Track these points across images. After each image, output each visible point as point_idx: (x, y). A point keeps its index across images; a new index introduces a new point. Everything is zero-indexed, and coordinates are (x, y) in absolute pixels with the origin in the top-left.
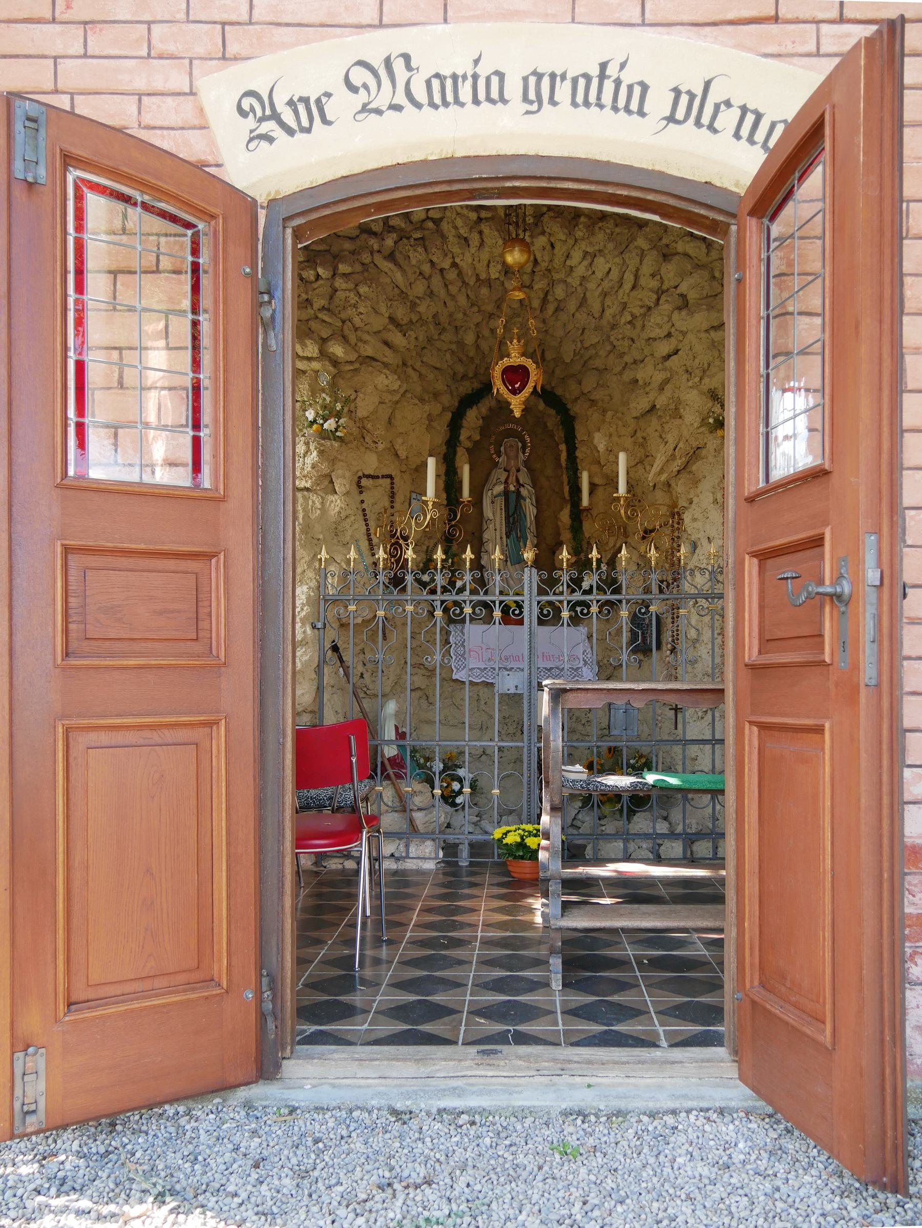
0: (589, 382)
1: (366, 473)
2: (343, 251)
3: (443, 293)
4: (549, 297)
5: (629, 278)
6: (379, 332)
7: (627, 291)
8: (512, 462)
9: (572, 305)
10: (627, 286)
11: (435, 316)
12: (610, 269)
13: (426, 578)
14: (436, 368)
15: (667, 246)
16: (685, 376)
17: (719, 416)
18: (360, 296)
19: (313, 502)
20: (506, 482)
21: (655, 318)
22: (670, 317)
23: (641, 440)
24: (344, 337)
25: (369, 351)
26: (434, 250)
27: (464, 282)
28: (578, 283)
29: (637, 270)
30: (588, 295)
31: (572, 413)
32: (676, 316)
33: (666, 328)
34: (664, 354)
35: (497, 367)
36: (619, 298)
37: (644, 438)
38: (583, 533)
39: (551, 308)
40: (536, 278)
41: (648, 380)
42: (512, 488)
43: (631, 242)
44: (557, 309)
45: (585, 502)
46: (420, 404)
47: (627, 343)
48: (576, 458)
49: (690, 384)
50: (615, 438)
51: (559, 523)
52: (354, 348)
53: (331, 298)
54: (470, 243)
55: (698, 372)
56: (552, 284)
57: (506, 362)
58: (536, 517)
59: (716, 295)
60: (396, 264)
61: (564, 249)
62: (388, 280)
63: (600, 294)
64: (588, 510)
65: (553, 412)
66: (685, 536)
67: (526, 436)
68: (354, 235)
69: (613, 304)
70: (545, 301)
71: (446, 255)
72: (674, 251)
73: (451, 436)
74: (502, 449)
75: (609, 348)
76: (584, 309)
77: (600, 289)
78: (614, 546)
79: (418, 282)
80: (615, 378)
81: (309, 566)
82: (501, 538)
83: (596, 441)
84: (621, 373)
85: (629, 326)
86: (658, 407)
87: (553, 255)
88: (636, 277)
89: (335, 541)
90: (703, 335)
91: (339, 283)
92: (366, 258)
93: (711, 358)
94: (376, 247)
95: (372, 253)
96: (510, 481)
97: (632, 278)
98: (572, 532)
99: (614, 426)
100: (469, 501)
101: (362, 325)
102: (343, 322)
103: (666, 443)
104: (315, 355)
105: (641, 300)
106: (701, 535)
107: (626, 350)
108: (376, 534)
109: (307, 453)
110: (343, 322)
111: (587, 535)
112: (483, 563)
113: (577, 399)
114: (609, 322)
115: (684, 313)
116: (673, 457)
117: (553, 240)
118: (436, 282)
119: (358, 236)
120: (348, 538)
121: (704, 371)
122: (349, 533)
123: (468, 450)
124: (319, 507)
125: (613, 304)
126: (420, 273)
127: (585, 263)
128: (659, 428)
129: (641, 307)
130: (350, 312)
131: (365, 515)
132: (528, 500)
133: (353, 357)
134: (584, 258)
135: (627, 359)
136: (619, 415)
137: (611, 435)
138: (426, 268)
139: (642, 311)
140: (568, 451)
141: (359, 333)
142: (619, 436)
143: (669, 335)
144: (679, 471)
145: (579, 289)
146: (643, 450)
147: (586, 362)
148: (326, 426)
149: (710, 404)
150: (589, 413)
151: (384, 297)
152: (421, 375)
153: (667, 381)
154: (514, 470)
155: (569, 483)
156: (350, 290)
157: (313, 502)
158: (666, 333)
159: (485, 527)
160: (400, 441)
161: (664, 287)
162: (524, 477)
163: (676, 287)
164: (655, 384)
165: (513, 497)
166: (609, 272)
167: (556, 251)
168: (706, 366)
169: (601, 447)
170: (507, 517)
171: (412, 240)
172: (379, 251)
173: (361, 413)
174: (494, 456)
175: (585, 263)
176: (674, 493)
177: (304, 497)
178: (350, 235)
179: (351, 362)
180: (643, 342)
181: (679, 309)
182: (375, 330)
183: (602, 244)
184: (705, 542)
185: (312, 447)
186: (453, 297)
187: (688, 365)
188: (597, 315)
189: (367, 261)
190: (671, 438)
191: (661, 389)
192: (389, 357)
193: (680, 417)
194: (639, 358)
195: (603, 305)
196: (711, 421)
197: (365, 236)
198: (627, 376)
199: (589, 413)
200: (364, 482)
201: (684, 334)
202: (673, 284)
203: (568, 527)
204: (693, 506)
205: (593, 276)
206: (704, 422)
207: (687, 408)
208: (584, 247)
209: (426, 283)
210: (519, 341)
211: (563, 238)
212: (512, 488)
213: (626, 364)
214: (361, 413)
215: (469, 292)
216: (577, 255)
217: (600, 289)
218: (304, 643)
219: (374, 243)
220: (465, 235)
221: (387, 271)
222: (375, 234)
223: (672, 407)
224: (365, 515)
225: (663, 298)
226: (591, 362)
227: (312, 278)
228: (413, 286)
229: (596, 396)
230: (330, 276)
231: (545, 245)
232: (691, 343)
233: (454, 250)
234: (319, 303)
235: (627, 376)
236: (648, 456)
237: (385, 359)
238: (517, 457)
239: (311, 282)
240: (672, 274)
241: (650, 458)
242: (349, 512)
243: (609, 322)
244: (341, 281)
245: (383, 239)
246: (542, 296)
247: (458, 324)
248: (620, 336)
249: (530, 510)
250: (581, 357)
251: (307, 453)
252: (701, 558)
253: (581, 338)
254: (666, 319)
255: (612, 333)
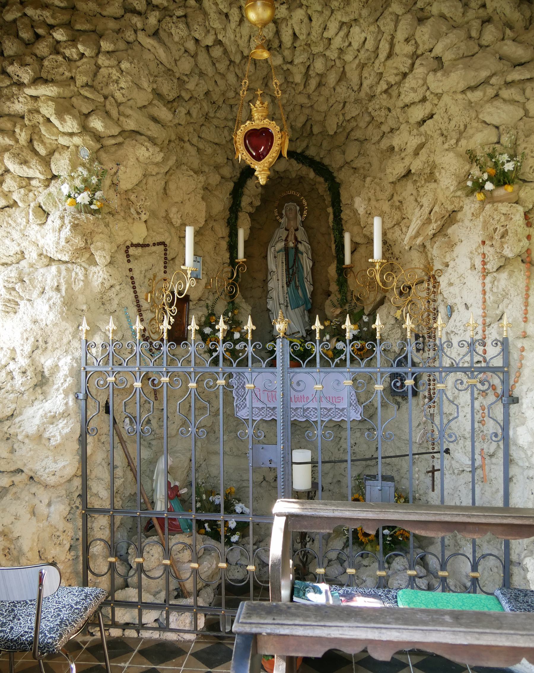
0: (352, 151)
1: (135, 242)
2: (107, 29)
3: (210, 71)
4: (311, 72)
5: (384, 47)
6: (144, 107)
7: (383, 60)
8: (292, 223)
9: (332, 78)
10: (383, 55)
11: (207, 93)
12: (366, 39)
13: (207, 330)
14: (216, 144)
15: (422, 9)
16: (441, 139)
17: (478, 178)
18: (122, 71)
19: (77, 274)
20: (286, 240)
21: (410, 82)
22: (425, 80)
23: (398, 204)
24: (107, 112)
25: (131, 125)
26: (196, 26)
27: (231, 61)
28: (336, 55)
29: (393, 37)
30: (347, 68)
31: (337, 180)
32: (431, 78)
33: (421, 92)
34: (419, 119)
35: (239, 132)
36: (375, 69)
37: (401, 202)
38: (347, 287)
39: (313, 83)
40: (297, 53)
41: (403, 147)
42: (291, 245)
43: (386, 8)
44: (320, 85)
45: (347, 261)
46: (195, 176)
47: (383, 113)
48: (341, 219)
49: (446, 146)
50: (373, 203)
51: (329, 276)
52: (117, 122)
53: (95, 75)
54: (231, 18)
55: (455, 135)
56: (313, 57)
57: (249, 126)
58: (312, 269)
59: (473, 56)
60: (161, 41)
61: (321, 20)
62: (151, 57)
63: (358, 65)
64: (350, 268)
65: (322, 180)
66: (440, 298)
67: (304, 201)
68: (118, 15)
69: (370, 75)
70: (307, 76)
71: (208, 31)
72: (429, 15)
73: (233, 202)
74: (284, 212)
75: (367, 119)
76: (344, 83)
77: (357, 61)
78: (375, 300)
79: (183, 59)
80: (373, 148)
81: (74, 337)
82: (283, 287)
83: (356, 205)
84: (379, 142)
85: (385, 96)
86: (413, 171)
87: (311, 27)
88: (392, 45)
89: (102, 310)
90: (460, 96)
91: (102, 60)
92: (130, 35)
93: (468, 120)
94: (139, 25)
95: (135, 31)
96: (289, 239)
97: (387, 46)
98: (338, 285)
99: (373, 191)
100: (243, 262)
101: (124, 100)
102: (106, 98)
103: (422, 206)
104: (75, 131)
105: (396, 68)
106: (458, 301)
107: (383, 120)
108: (147, 300)
109: (62, 226)
110: (106, 98)
111: (351, 288)
112: (269, 307)
113: (341, 168)
114: (367, 94)
115: (439, 74)
116: (428, 221)
117: (309, 12)
118: (203, 59)
119: (123, 16)
120: (115, 306)
121: (461, 133)
122: (115, 302)
123: (250, 214)
124: (82, 278)
125: (370, 75)
126: (186, 51)
127: (342, 34)
128: (415, 193)
129: (397, 75)
130: (113, 87)
131: (133, 283)
132: (305, 255)
133: (115, 131)
134: (340, 28)
135: (385, 128)
136: (377, 180)
137: (370, 200)
138: (190, 45)
139: (398, 78)
140: (334, 214)
141: (122, 108)
142: (377, 200)
143: (424, 100)
144: (434, 235)
145: (337, 61)
146: (399, 213)
147: (348, 134)
148: (79, 200)
149: (467, 167)
150: (351, 180)
151: (146, 72)
152: (199, 150)
153: (421, 146)
154: (292, 230)
155: (335, 241)
156: (112, 67)
157: (77, 274)
158: (420, 97)
159: (269, 278)
160: (174, 210)
161: (419, 52)
162: (301, 235)
163: (431, 51)
164: (410, 150)
165: (292, 253)
166: (364, 42)
167: (314, 23)
168: (462, 127)
169: (361, 211)
170: (287, 270)
171: (175, 18)
172: (143, 30)
173: (124, 185)
174: (278, 218)
175: (342, 34)
176: (430, 255)
177: (67, 269)
178: (115, 16)
179: (113, 136)
180: (399, 110)
181: (435, 71)
182: (139, 105)
183: (357, 12)
184: (462, 308)
185: (67, 221)
186: (223, 76)
187: (443, 128)
188: (356, 88)
189: (131, 39)
190: (426, 201)
191: (416, 153)
192: (154, 130)
193: (435, 181)
194: (395, 126)
195: (361, 77)
196: (469, 183)
197: (128, 15)
198: (385, 144)
199: (351, 180)
200: (132, 251)
201: (439, 96)
202: (427, 47)
203: (335, 280)
204: (450, 270)
205: (350, 48)
206: (461, 184)
207: (443, 171)
208: (339, 17)
209: (192, 60)
210: (262, 103)
211: (319, 8)
212: (291, 245)
213: (384, 133)
214: (124, 185)
215: (237, 71)
216: (333, 27)
217: (357, 61)
218: (66, 415)
219: (136, 21)
220: (225, 11)
221: (150, 48)
222: (139, 13)
223: (428, 171)
224: (133, 283)
225: (418, 62)
226: (353, 133)
227: (75, 56)
228: (178, 63)
229: (357, 164)
230: (93, 54)
231: (302, 17)
232: (446, 105)
233: (215, 26)
234: (81, 79)
235: (385, 144)
236: (404, 218)
237: (149, 133)
238: (296, 218)
239: (75, 61)
240: (427, 36)
241: (406, 220)
242: (112, 282)
243: (367, 94)
244: (104, 58)
245: (147, 18)
246: (304, 71)
247: (232, 102)
248: (377, 107)
249: (307, 263)
250: (344, 130)
251: (62, 226)
252: (458, 324)
253: (343, 112)
254: (421, 82)
255: (370, 104)
